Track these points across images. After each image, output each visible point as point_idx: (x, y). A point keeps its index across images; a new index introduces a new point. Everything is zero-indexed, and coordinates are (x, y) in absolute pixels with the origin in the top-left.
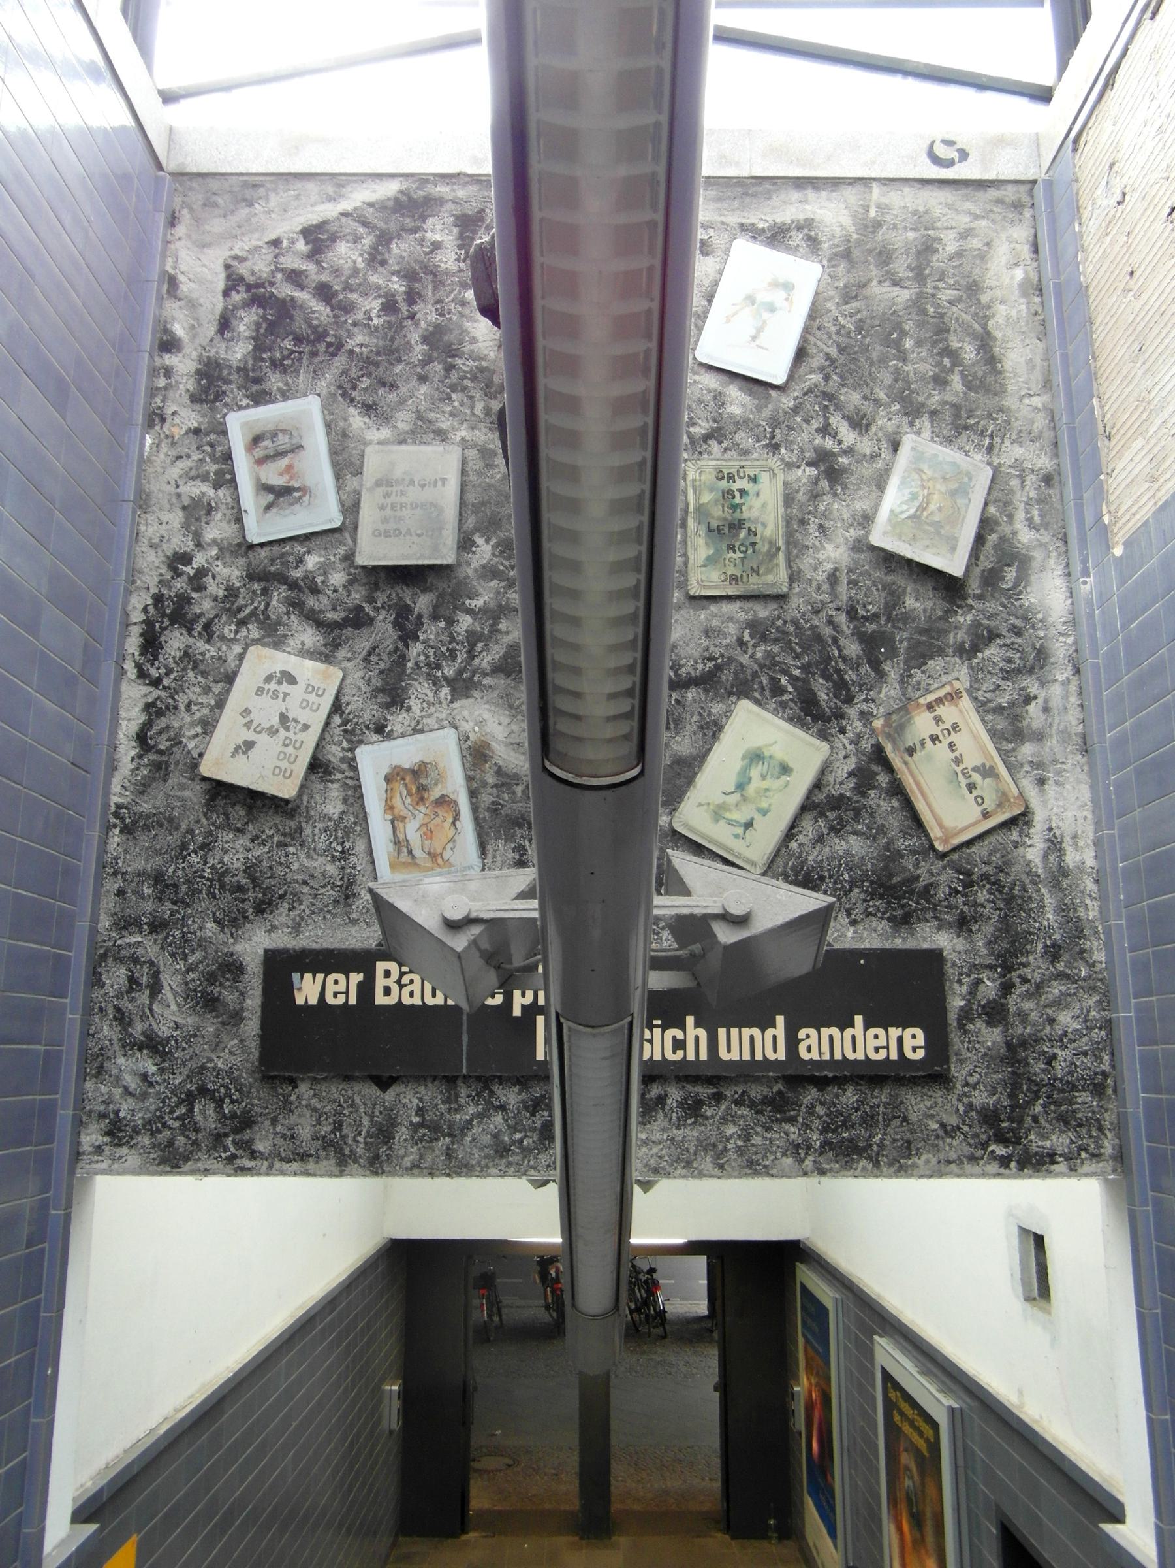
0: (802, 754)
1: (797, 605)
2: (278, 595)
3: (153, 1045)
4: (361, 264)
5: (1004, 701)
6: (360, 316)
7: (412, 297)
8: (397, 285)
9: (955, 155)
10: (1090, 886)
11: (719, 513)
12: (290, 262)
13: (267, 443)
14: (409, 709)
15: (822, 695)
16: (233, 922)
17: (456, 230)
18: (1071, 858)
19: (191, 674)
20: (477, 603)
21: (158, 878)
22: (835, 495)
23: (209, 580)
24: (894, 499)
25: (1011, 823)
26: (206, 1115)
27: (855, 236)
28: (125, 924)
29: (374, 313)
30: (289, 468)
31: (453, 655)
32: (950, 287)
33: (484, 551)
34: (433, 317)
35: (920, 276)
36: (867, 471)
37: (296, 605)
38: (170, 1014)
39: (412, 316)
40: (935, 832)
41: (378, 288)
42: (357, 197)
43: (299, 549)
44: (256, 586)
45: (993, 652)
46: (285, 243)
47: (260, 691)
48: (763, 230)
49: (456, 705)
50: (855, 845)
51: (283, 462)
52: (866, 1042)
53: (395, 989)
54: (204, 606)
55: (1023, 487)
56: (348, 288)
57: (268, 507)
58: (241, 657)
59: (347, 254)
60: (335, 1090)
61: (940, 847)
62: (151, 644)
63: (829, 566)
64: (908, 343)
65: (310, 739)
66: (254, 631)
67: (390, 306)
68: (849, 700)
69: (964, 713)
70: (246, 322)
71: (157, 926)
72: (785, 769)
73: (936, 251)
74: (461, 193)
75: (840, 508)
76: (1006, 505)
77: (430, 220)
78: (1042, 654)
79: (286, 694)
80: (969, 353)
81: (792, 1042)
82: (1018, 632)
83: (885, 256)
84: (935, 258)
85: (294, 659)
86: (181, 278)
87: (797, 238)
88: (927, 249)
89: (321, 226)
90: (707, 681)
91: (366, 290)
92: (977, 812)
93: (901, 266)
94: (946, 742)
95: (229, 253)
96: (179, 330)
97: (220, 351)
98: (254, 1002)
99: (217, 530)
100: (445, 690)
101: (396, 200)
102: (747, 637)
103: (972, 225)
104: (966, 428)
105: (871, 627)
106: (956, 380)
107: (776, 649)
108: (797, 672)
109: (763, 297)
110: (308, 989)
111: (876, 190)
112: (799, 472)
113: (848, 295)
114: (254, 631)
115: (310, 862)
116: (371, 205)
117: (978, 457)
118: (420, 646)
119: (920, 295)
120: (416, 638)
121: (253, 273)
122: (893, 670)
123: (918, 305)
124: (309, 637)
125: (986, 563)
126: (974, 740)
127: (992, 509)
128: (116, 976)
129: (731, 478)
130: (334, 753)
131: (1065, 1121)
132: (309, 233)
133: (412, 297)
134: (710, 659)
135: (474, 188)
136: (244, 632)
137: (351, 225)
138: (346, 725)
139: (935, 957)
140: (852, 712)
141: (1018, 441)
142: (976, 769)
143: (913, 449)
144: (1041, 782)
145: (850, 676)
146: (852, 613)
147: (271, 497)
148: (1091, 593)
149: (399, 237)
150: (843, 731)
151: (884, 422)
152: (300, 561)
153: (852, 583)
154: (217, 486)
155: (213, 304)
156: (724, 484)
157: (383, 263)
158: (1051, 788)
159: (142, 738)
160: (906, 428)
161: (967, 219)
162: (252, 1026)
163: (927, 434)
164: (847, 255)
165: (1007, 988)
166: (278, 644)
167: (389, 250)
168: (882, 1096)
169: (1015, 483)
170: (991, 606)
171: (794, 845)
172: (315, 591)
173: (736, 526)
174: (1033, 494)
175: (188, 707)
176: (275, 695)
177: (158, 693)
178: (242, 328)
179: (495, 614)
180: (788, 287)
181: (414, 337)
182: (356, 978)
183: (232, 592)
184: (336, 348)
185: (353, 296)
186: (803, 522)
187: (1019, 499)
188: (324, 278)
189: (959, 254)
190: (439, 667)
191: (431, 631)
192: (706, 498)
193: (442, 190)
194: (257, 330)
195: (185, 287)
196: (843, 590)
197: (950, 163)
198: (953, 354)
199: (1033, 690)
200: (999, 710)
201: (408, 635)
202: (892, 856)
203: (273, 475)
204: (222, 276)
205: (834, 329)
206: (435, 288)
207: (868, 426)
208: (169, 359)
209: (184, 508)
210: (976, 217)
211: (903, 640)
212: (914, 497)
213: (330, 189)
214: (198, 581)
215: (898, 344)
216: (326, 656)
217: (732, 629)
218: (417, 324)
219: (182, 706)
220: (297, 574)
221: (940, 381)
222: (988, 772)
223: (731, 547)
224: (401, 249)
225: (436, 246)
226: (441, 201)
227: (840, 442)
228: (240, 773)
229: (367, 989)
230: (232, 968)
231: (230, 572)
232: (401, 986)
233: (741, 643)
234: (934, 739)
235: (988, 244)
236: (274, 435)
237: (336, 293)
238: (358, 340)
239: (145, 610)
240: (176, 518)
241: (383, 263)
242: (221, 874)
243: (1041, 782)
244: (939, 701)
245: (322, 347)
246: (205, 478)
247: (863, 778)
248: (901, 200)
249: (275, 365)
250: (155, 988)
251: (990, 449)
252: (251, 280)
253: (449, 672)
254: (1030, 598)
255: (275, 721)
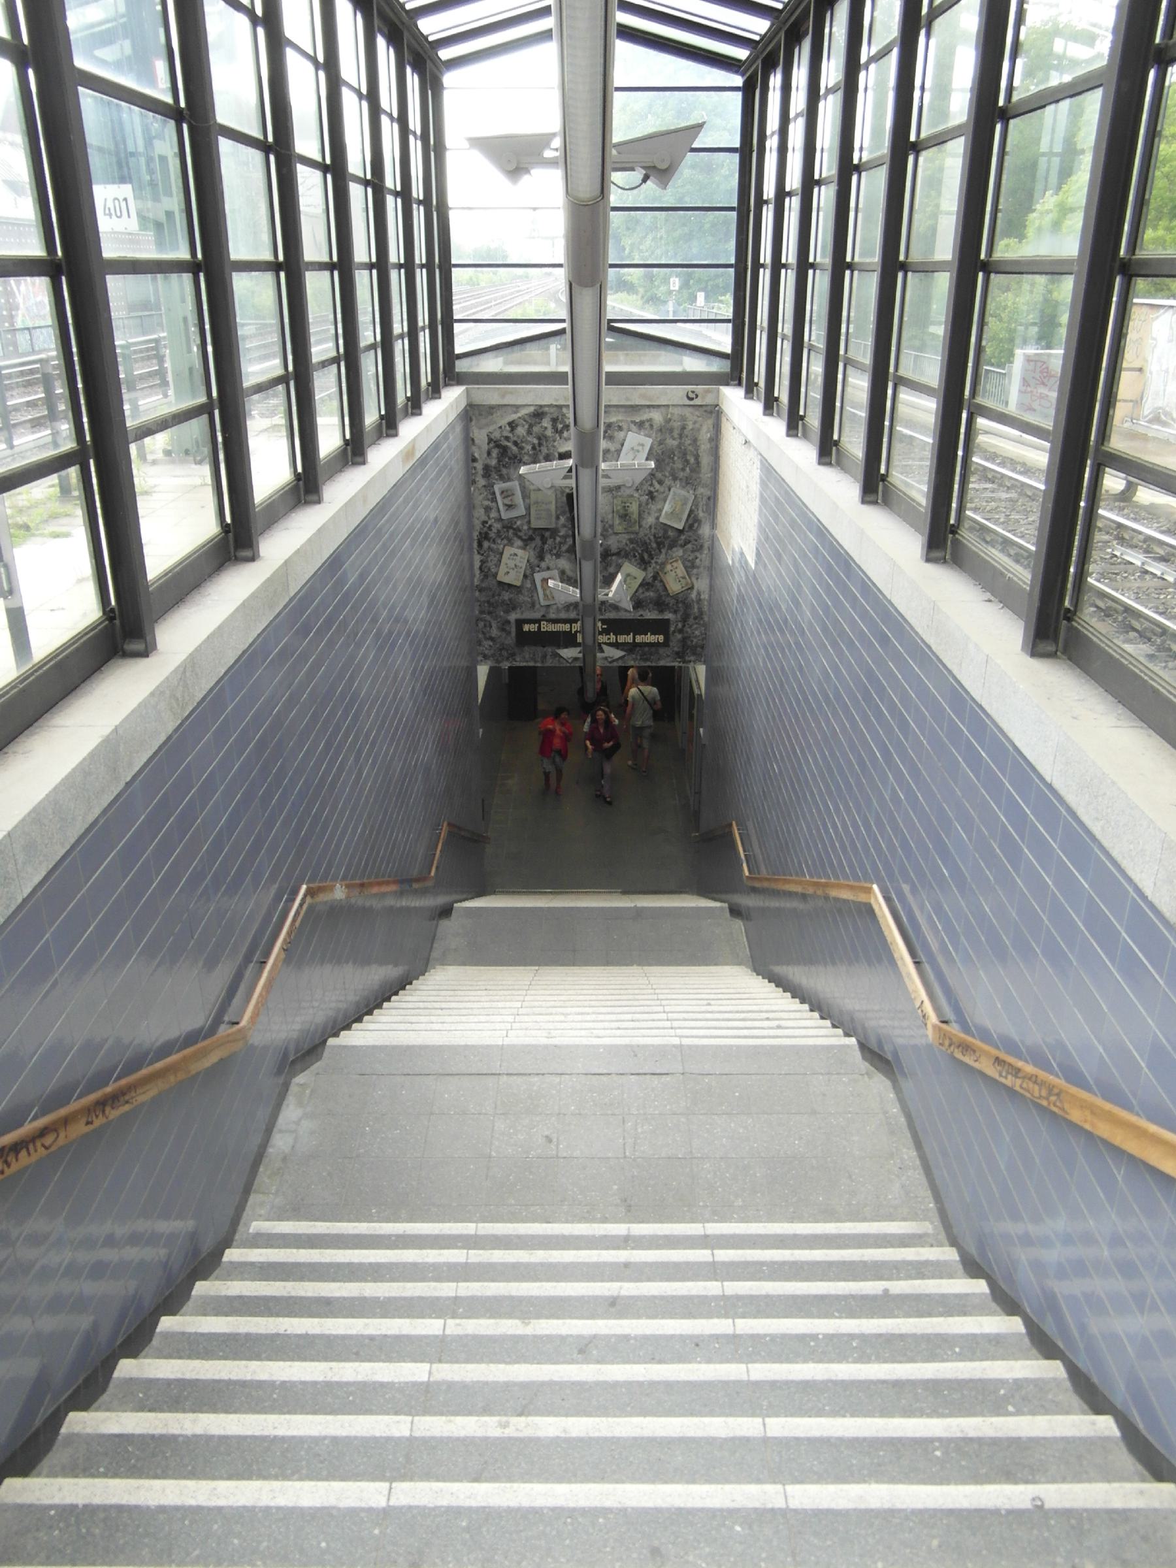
0: (640, 575)
1: (641, 534)
2: (511, 531)
3: (492, 639)
7: (540, 445)
8: (536, 441)
11: (622, 512)
12: (506, 434)
16: (507, 612)
21: (488, 602)
24: (667, 508)
26: (505, 653)
28: (482, 612)
35: (681, 436)
36: (662, 496)
37: (516, 535)
38: (495, 632)
42: (523, 412)
45: (689, 546)
52: (650, 638)
54: (492, 535)
59: (521, 431)
60: (533, 648)
62: (480, 545)
65: (522, 571)
66: (505, 541)
67: (534, 448)
69: (680, 565)
70: (495, 453)
71: (490, 613)
75: (653, 507)
76: (697, 506)
78: (702, 546)
80: (692, 460)
81: (634, 638)
83: (671, 430)
88: (683, 428)
90: (618, 554)
91: (527, 442)
93: (676, 434)
96: (476, 455)
97: (488, 461)
98: (513, 630)
99: (493, 514)
110: (526, 628)
113: (660, 443)
115: (524, 598)
122: (663, 551)
123: (679, 446)
124: (519, 543)
125: (690, 522)
128: (481, 624)
130: (528, 572)
131: (694, 654)
132: (510, 424)
133: (540, 445)
138: (532, 568)
139: (668, 620)
148: (60, 1265)
151: (668, 482)
155: (485, 447)
159: (481, 568)
162: (513, 634)
168: (653, 649)
170: (690, 534)
173: (626, 515)
179: (565, 537)
180: (643, 445)
183: (499, 531)
191: (550, 541)
193: (546, 409)
195: (477, 441)
197: (692, 399)
198: (687, 461)
202: (660, 596)
203: (507, 501)
208: (475, 464)
211: (667, 543)
214: (490, 528)
216: (524, 548)
221: (683, 470)
222: (684, 578)
224: (536, 429)
228: (506, 580)
229: (539, 627)
230: (508, 622)
231: (497, 526)
240: (482, 511)
242: (503, 601)
247: (655, 577)
248: (677, 411)
254: (700, 532)
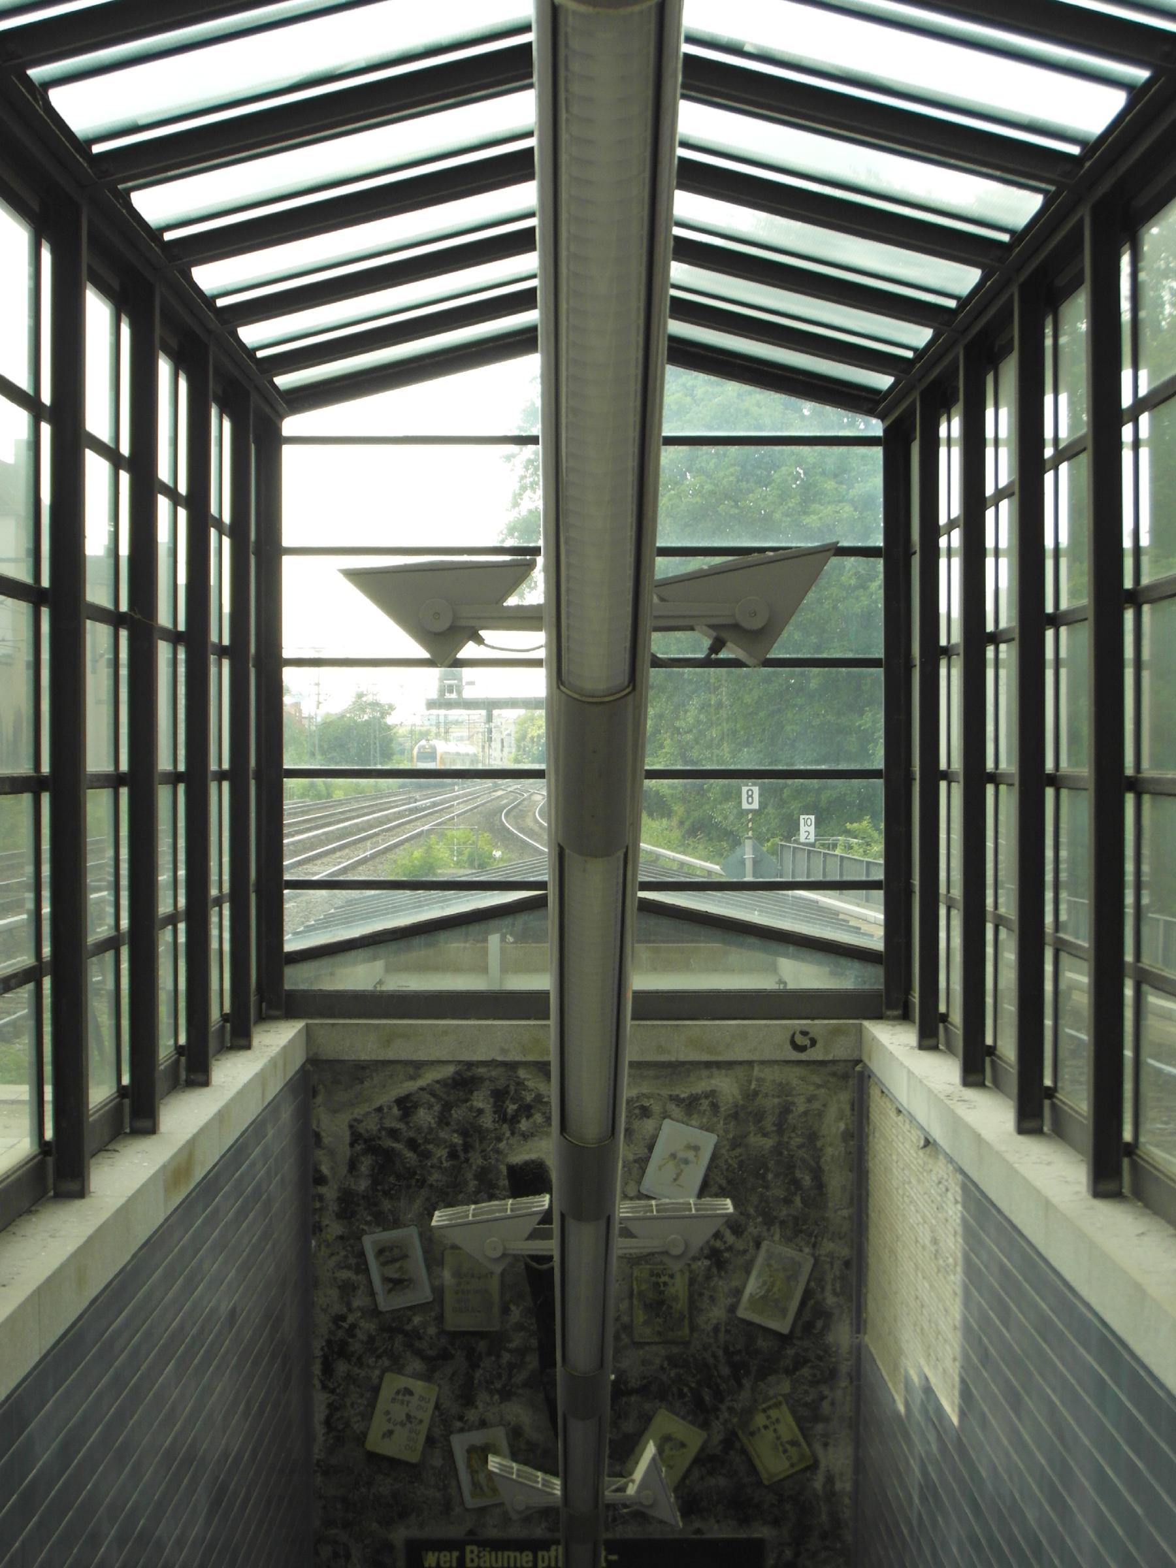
4: (434, 1126)
5: (809, 1399)
6: (435, 1161)
7: (467, 1147)
8: (457, 1140)
9: (808, 1042)
10: (847, 1501)
12: (390, 1123)
13: (387, 1253)
14: (476, 1407)
15: (707, 1398)
17: (491, 1100)
18: (838, 1486)
19: (352, 1387)
20: (513, 1345)
22: (720, 1277)
23: (358, 1331)
25: (807, 1468)
27: (741, 1102)
29: (443, 1159)
30: (401, 1268)
31: (500, 1376)
32: (798, 1136)
33: (516, 1314)
34: (480, 1161)
39: (467, 1160)
40: (764, 1475)
41: (445, 1142)
42: (430, 1077)
43: (410, 1313)
44: (386, 1335)
45: (805, 1371)
46: (386, 1110)
47: (394, 1400)
48: (684, 1099)
49: (503, 1406)
50: (722, 1481)
51: (397, 1265)
53: (476, 1560)
54: (356, 1346)
55: (832, 1268)
56: (427, 1141)
57: (390, 1291)
58: (381, 1378)
59: (425, 1117)
61: (766, 1483)
62: (328, 1369)
63: (715, 1321)
64: (770, 1176)
66: (386, 1362)
67: (453, 1155)
68: (722, 1401)
72: (683, 1445)
73: (790, 1111)
74: (494, 1073)
75: (722, 1285)
76: (821, 1281)
77: (475, 1093)
78: (833, 1373)
79: (408, 1402)
80: (807, 1181)
82: (820, 1358)
83: (759, 1116)
84: (790, 1116)
85: (411, 1380)
86: (323, 1134)
87: (705, 1104)
88: (786, 1110)
89: (408, 1097)
90: (643, 1391)
91: (438, 1142)
92: (787, 1464)
93: (769, 1123)
94: (772, 1428)
95: (351, 1117)
96: (325, 1169)
100: (496, 1397)
101: (453, 1079)
102: (666, 1364)
103: (816, 1092)
104: (801, 1231)
105: (737, 1358)
106: (798, 1200)
107: (681, 1371)
108: (693, 1385)
109: (681, 1155)
111: (756, 1071)
112: (700, 1263)
113: (735, 1144)
114: (386, 1362)
116: (438, 1082)
117: (807, 1250)
118: (481, 1371)
119: (779, 1143)
120: (479, 1366)
121: (367, 1131)
123: (777, 1150)
124: (416, 1365)
126: (787, 1426)
127: (813, 1284)
129: (658, 1276)
130: (437, 1432)
133: (467, 1147)
134: (644, 1378)
135: (503, 1069)
136: (380, 1362)
137: (426, 1097)
138: (445, 1423)
139: (760, 1542)
140: (723, 1407)
141: (832, 1240)
142: (788, 1442)
143: (767, 1251)
144: (826, 1445)
145: (723, 1387)
146: (726, 1350)
147: (391, 1285)
149: (457, 1106)
150: (717, 1418)
152: (410, 1320)
153: (727, 1332)
154: (357, 1272)
156: (654, 1279)
157: (448, 1124)
158: (831, 1449)
159: (328, 1422)
160: (765, 1234)
161: (812, 1088)
163: (777, 1237)
164: (735, 1116)
165: (797, 1554)
166: (400, 1370)
167: (451, 1115)
169: (827, 1267)
171: (687, 1482)
172: (420, 1338)
173: (661, 1303)
174: (838, 1273)
175: (352, 1404)
176: (402, 1402)
177: (333, 1397)
178: (363, 1169)
180: (696, 1149)
181: (469, 1176)
182: (455, 1554)
183: (371, 1339)
184: (422, 1183)
185: (430, 1147)
186: (701, 1295)
187: (829, 1277)
188: (412, 1134)
189: (805, 1113)
190: (492, 1383)
192: (644, 1287)
193: (482, 1071)
194: (373, 1170)
195: (326, 1140)
196: (722, 1336)
198: (796, 1183)
199: (826, 1392)
200: (806, 1405)
201: (474, 1364)
203: (392, 1272)
204: (348, 1133)
205: (725, 1167)
206: (481, 1142)
207: (742, 1233)
208: (322, 1190)
209: (339, 1287)
210: (818, 1086)
212: (765, 1283)
213: (411, 1071)
215: (763, 1177)
216: (427, 1377)
217: (658, 1361)
218: (471, 1166)
219: (348, 1404)
220: (408, 1327)
221: (788, 1201)
222: (794, 1443)
223: (658, 1315)
224: (457, 1114)
225: (480, 1112)
226: (481, 1080)
227: (725, 1243)
230: (389, 1546)
231: (368, 1326)
232: (479, 1558)
233: (662, 1368)
234: (766, 1427)
235: (824, 1105)
236: (391, 1249)
237: (419, 1145)
238: (435, 1177)
239: (322, 1349)
240: (334, 1293)
241: (448, 1124)
243: (826, 1445)
244: (769, 1407)
245: (413, 1182)
246: (349, 1267)
248: (771, 1075)
249: (386, 1194)
250: (348, 1557)
251: (814, 1246)
252: (366, 1135)
253: (498, 1385)
254: (830, 1339)
255: (404, 1418)
